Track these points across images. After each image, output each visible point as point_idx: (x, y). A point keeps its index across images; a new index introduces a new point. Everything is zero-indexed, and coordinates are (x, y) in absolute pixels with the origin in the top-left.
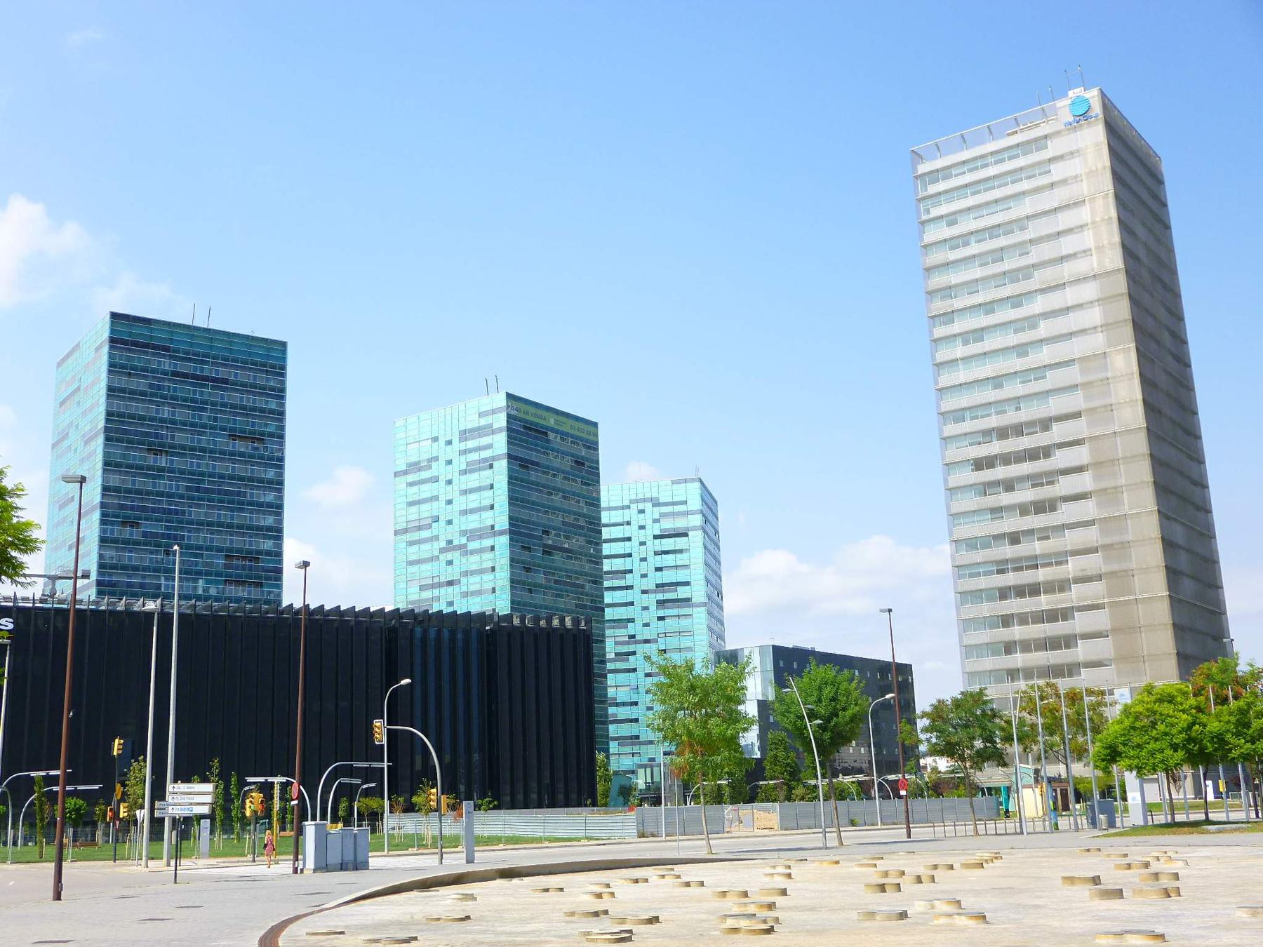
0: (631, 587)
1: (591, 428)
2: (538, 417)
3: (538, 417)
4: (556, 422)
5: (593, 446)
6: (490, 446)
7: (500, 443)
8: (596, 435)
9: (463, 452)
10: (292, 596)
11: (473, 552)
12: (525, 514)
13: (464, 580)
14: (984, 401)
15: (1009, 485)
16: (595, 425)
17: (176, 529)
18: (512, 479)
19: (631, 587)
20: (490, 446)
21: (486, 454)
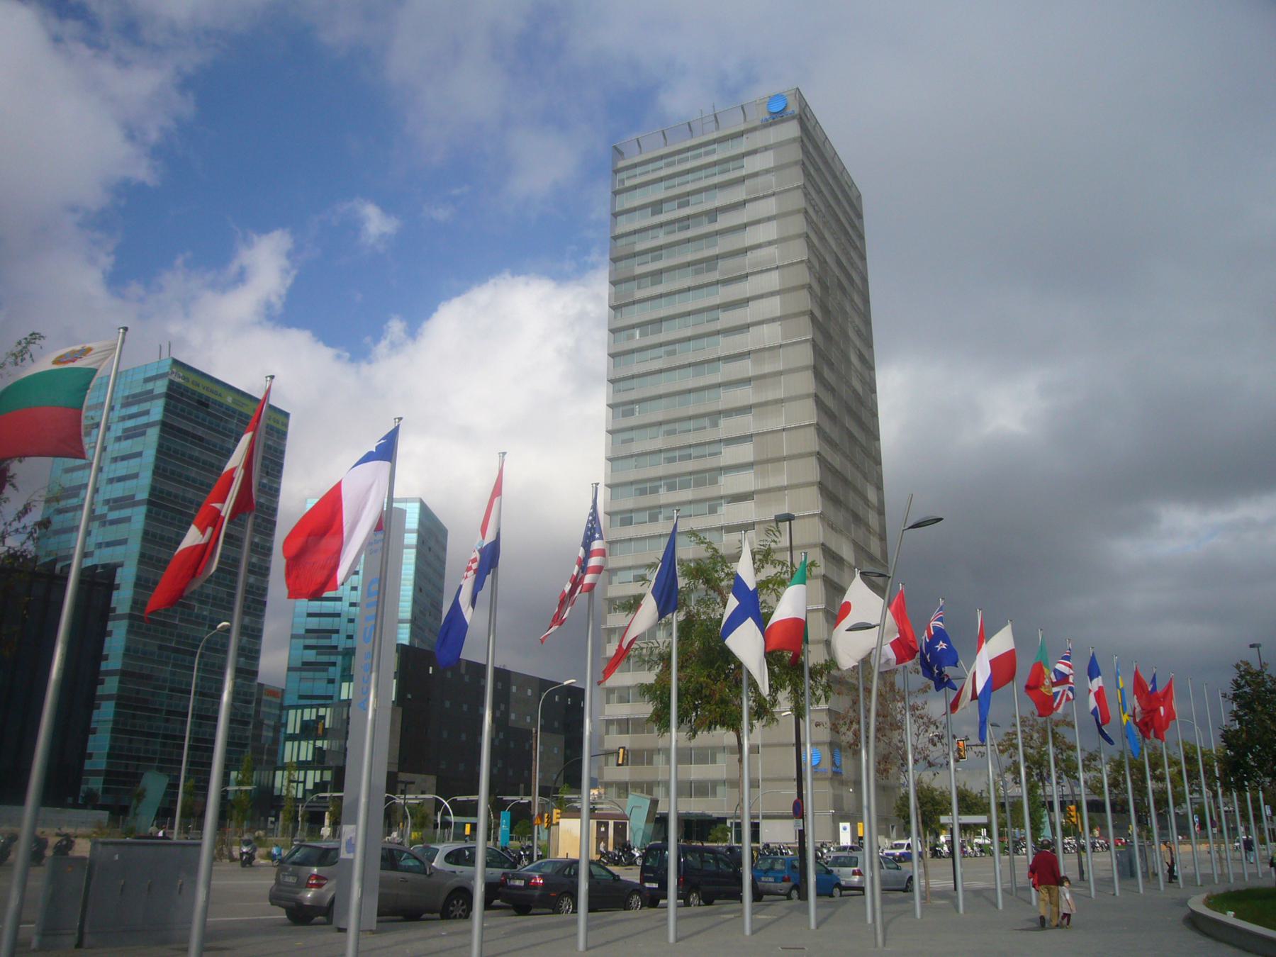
0: (340, 599)
1: (281, 418)
2: (212, 391)
3: (212, 391)
4: (234, 401)
5: (283, 435)
6: (147, 413)
7: (157, 410)
8: (286, 425)
9: (123, 419)
10: (465, 655)
11: (113, 522)
12: (171, 487)
13: (97, 552)
14: (740, 376)
15: (819, 192)
16: (287, 415)
17: (1162, 818)
18: (162, 451)
19: (340, 599)
20: (147, 413)
21: (143, 420)
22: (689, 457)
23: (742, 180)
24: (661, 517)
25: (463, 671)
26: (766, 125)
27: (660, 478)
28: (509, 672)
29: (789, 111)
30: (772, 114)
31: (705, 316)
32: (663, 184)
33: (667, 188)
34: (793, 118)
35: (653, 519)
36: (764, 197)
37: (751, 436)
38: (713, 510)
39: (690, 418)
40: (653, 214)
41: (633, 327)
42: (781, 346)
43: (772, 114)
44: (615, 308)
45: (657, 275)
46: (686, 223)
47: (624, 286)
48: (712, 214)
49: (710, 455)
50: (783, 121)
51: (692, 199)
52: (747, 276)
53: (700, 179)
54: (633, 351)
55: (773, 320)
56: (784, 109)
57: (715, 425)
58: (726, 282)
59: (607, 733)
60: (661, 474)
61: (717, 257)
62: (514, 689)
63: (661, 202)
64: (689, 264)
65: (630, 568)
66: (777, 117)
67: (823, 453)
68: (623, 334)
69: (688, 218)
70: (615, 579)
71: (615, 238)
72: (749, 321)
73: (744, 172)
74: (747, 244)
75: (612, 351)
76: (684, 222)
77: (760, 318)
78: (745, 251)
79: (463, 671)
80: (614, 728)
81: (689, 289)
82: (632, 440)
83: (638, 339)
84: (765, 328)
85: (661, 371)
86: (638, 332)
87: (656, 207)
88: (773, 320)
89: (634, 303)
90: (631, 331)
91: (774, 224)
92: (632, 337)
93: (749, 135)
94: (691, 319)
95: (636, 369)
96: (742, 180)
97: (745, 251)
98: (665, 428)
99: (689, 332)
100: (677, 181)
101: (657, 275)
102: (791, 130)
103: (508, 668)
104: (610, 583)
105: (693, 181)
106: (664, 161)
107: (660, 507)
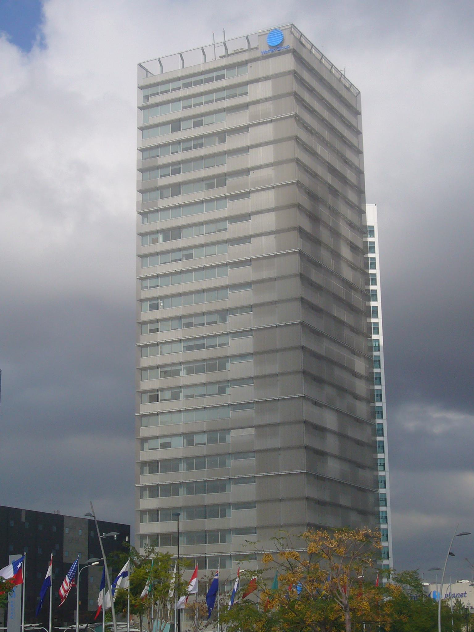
22: (203, 346)
23: (245, 106)
24: (181, 395)
25: (23, 519)
26: (266, 57)
27: (180, 364)
28: (62, 517)
29: (285, 45)
30: (271, 47)
31: (216, 226)
32: (181, 104)
33: (185, 108)
34: (288, 51)
35: (175, 397)
36: (264, 123)
37: (250, 260)
38: (222, 391)
39: (203, 314)
40: (173, 131)
41: (157, 232)
42: (275, 256)
43: (271, 47)
44: (144, 214)
45: (176, 189)
46: (200, 141)
47: (149, 195)
48: (222, 136)
49: (220, 345)
50: (280, 54)
51: (206, 119)
52: (249, 193)
53: (212, 101)
54: (157, 254)
55: (267, 143)
56: (282, 43)
57: (224, 320)
58: (233, 197)
59: (142, 473)
60: (181, 360)
61: (225, 175)
62: (66, 531)
63: (179, 121)
64: (202, 180)
65: (157, 437)
66: (276, 50)
67: (299, 71)
68: (149, 238)
69: (202, 137)
70: (146, 446)
71: (142, 279)
72: (250, 211)
73: (247, 99)
74: (250, 165)
75: (141, 85)
76: (198, 142)
77: (259, 141)
78: (247, 171)
79: (23, 519)
80: (147, 517)
81: (202, 202)
82: (157, 330)
83: (162, 245)
84: (264, 240)
85: (180, 272)
86: (161, 237)
87: (176, 125)
88: (267, 143)
89: (158, 211)
90: (155, 236)
91: (269, 83)
92: (156, 241)
93: (253, 64)
94: (204, 228)
95: (161, 269)
96: (245, 106)
97: (247, 171)
98: (183, 145)
99: (201, 240)
100: (193, 101)
101: (176, 189)
102: (286, 63)
103: (61, 514)
104: (142, 449)
105: (207, 103)
106: (181, 82)
107: (181, 387)
